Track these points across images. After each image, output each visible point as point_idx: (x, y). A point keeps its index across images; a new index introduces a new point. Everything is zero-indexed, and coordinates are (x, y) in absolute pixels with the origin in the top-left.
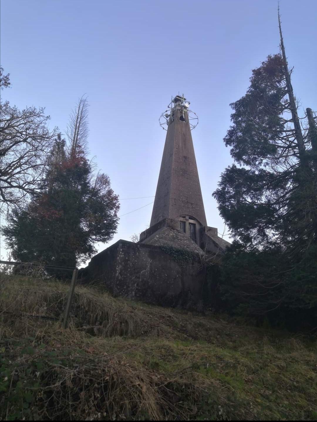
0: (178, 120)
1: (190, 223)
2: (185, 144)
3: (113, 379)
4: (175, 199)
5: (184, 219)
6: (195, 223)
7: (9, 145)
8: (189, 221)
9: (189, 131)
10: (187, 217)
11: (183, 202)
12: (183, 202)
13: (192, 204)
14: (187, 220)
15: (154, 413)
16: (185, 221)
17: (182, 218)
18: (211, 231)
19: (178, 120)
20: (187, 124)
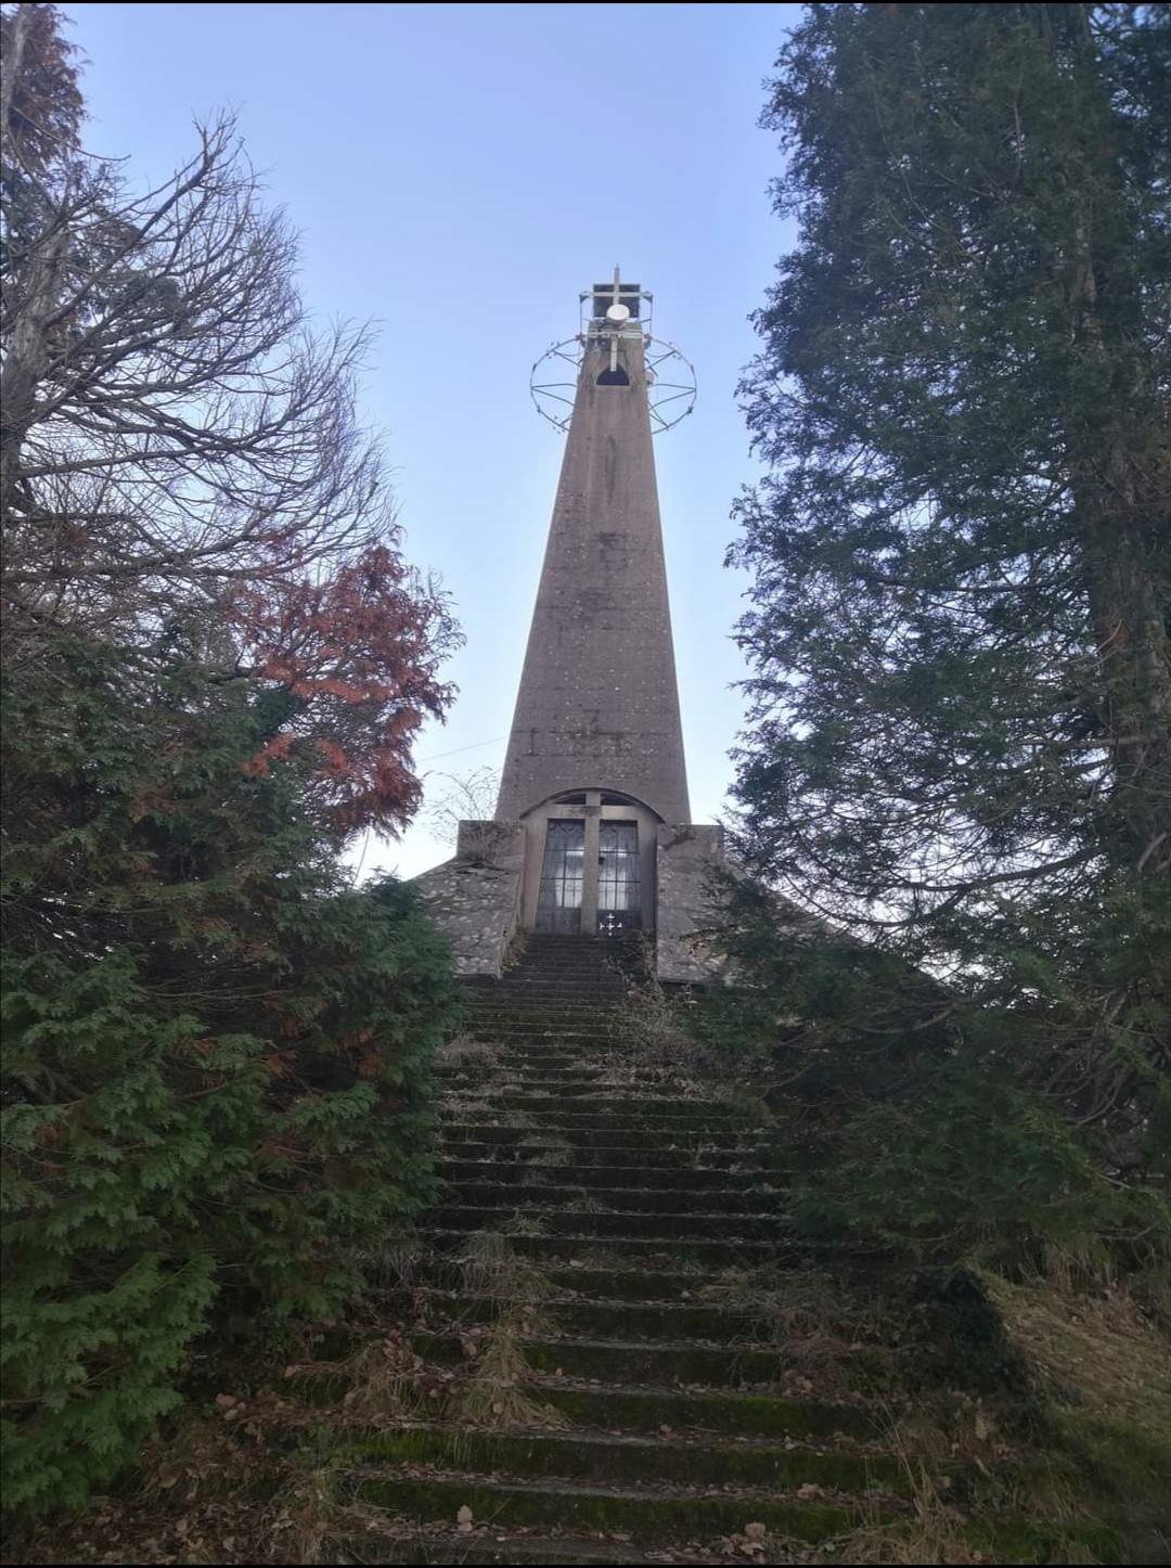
0: (612, 378)
1: (604, 823)
2: (611, 485)
3: (286, 704)
4: (534, 731)
5: (578, 807)
6: (630, 817)
7: (235, 1406)
8: (600, 812)
9: (645, 436)
10: (593, 800)
11: (573, 737)
12: (573, 737)
13: (618, 736)
14: (592, 811)
15: (12, 1502)
16: (581, 817)
17: (569, 807)
18: (688, 842)
19: (612, 378)
20: (639, 410)
